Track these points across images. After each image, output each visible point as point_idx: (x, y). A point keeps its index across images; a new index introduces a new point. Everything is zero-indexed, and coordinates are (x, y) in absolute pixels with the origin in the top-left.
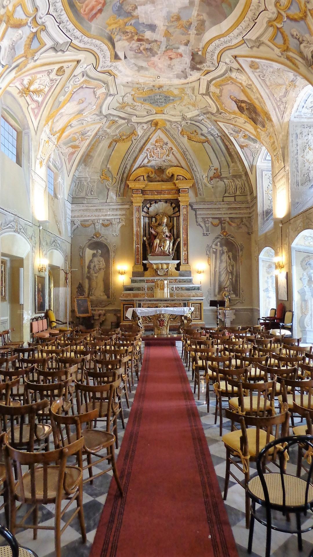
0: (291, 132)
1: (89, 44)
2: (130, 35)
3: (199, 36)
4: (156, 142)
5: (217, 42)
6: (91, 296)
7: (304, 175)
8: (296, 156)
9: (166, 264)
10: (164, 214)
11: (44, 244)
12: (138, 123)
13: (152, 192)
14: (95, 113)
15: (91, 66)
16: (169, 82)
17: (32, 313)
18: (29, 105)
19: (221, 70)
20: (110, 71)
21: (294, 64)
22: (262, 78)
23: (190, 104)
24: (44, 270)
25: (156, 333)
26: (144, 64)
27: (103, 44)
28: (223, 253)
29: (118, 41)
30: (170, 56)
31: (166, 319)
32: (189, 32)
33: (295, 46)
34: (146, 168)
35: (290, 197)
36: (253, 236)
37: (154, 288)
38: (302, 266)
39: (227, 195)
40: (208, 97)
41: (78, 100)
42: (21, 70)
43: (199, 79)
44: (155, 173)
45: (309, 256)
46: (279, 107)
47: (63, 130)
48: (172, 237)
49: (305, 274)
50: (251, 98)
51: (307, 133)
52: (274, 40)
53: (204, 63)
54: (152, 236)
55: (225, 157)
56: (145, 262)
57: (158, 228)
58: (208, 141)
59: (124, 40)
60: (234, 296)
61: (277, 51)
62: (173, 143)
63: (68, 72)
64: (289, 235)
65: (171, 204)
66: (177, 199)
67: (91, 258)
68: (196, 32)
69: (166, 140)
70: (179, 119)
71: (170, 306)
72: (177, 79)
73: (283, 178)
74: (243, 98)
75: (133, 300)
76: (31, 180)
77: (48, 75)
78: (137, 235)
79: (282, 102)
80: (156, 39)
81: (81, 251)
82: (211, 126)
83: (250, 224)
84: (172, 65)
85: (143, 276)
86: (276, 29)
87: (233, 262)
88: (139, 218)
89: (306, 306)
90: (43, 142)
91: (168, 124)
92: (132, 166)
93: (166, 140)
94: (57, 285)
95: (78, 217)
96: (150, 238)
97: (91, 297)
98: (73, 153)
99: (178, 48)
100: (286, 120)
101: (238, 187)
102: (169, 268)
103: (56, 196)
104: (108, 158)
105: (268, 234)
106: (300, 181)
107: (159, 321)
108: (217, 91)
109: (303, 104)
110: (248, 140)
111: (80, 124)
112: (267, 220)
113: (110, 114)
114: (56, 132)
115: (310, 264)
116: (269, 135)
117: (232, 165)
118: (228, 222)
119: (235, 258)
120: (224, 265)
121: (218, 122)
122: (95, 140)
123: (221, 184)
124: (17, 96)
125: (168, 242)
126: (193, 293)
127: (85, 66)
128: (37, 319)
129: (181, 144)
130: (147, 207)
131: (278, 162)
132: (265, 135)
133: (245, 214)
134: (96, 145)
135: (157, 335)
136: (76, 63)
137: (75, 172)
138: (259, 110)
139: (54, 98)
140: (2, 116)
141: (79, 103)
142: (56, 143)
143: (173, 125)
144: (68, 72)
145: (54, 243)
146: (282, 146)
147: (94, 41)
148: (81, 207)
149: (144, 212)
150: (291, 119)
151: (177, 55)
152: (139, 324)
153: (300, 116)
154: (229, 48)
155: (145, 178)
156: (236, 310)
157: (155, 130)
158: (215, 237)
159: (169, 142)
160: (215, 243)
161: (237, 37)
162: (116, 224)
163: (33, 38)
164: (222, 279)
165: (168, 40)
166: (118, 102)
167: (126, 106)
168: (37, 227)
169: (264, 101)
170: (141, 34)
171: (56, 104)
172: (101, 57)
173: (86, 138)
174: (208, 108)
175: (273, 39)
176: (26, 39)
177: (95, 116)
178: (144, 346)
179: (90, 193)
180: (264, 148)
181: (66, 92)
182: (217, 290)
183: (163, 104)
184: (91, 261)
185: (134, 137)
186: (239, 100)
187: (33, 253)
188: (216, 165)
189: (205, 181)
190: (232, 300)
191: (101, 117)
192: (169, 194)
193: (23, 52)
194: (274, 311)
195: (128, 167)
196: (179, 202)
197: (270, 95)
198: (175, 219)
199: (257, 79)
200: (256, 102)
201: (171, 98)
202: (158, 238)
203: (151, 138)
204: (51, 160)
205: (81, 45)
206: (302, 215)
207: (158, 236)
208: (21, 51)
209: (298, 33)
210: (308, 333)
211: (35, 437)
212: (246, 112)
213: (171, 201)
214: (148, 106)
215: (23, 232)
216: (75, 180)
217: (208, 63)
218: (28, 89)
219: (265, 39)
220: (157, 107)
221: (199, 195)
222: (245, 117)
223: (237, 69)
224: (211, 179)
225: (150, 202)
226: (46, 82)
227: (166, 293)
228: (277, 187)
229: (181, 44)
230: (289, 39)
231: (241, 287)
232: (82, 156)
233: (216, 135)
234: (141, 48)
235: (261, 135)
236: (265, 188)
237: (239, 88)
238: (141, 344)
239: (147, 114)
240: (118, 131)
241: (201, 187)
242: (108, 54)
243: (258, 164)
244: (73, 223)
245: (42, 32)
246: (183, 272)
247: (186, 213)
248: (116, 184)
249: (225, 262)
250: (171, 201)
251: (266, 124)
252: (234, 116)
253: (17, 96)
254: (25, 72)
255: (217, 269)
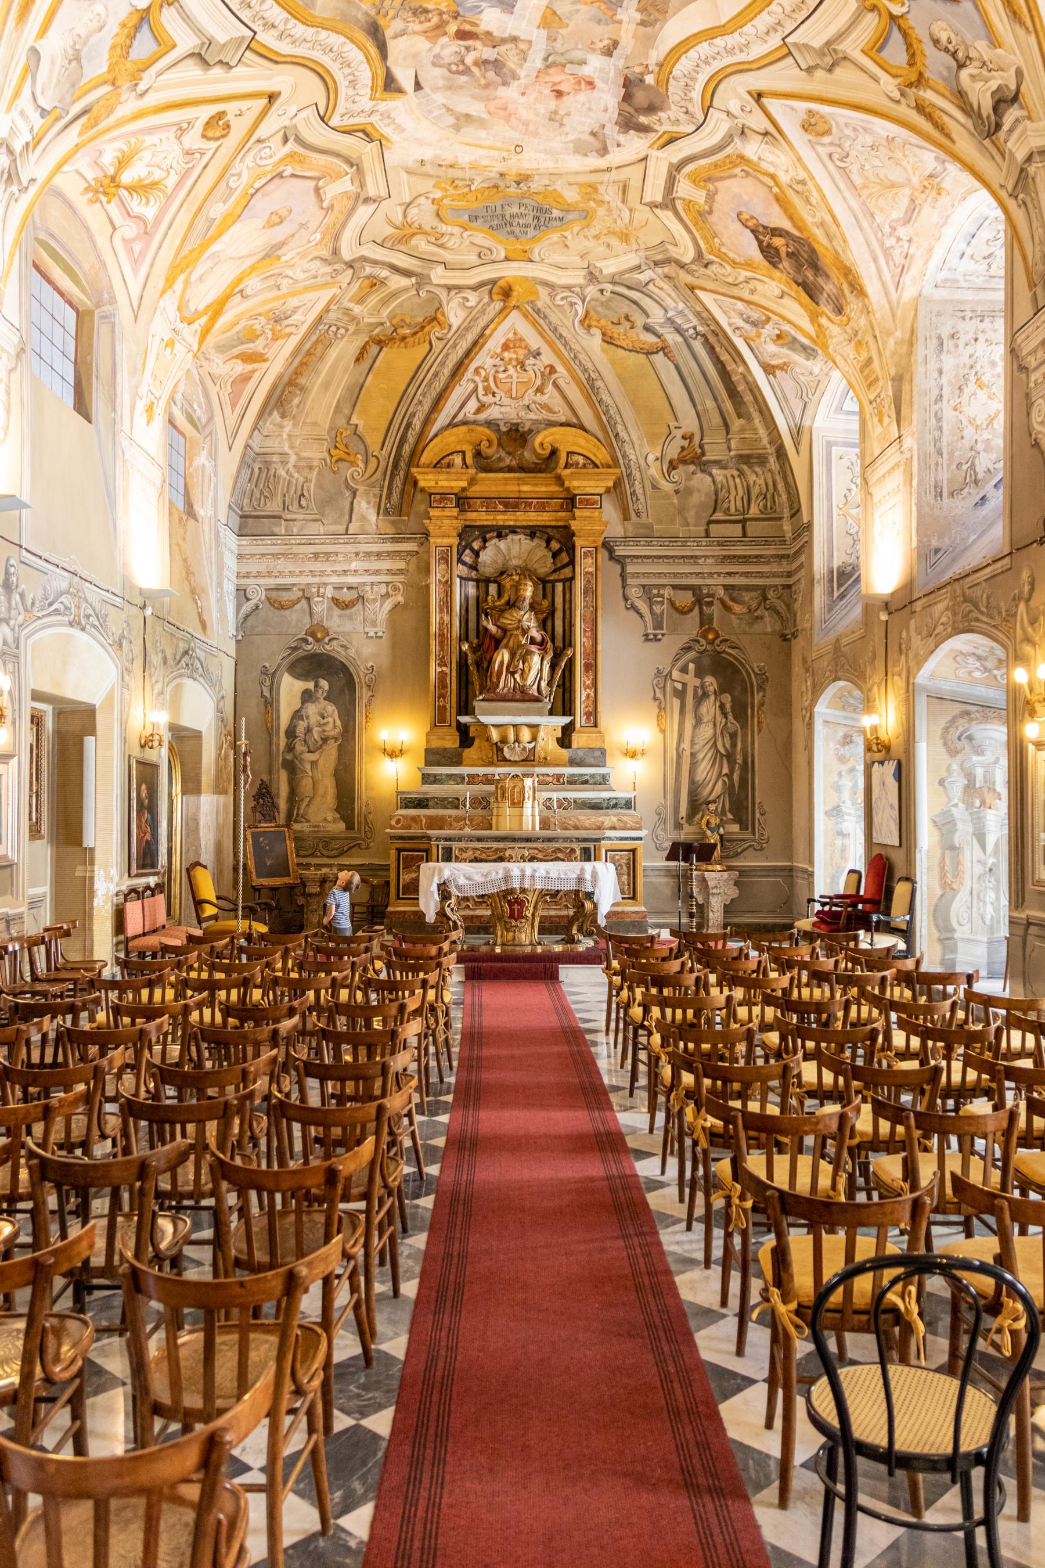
0: (921, 335)
1: (308, 45)
2: (435, 20)
3: (649, 29)
4: (506, 347)
5: (704, 49)
6: (296, 821)
7: (959, 465)
8: (937, 407)
9: (530, 726)
10: (526, 572)
11: (156, 659)
12: (449, 288)
13: (488, 502)
14: (316, 254)
15: (311, 112)
16: (548, 164)
17: (121, 878)
18: (114, 228)
19: (711, 134)
20: (369, 129)
21: (940, 128)
22: (839, 163)
23: (614, 233)
24: (156, 744)
25: (499, 941)
26: (476, 109)
27: (350, 46)
28: (705, 695)
29: (395, 37)
30: (555, 84)
31: (532, 898)
32: (618, 17)
33: (945, 73)
34: (471, 427)
35: (914, 531)
36: (798, 645)
37: (492, 800)
38: (945, 744)
39: (719, 516)
40: (670, 214)
41: (266, 215)
42: (96, 124)
43: (645, 159)
44: (500, 444)
45: (968, 713)
46: (887, 253)
47: (217, 309)
48: (550, 644)
49: (955, 767)
50: (803, 221)
51: (971, 335)
52: (880, 50)
53: (661, 109)
54: (487, 641)
55: (716, 399)
56: (464, 719)
57: (507, 615)
58: (664, 349)
59: (415, 33)
60: (735, 828)
61: (889, 85)
62: (557, 353)
63: (239, 128)
64: (908, 648)
65: (548, 542)
66: (567, 527)
67: (297, 705)
68: (638, 17)
69: (534, 341)
70: (577, 278)
71: (540, 856)
72: (577, 156)
73: (896, 472)
74: (777, 219)
75: (429, 838)
76: (119, 463)
77: (178, 138)
78: (442, 635)
79: (899, 239)
80: (515, 33)
81: (268, 683)
82: (675, 304)
83: (788, 606)
84: (562, 112)
85: (458, 762)
86: (885, 17)
87: (734, 725)
88: (448, 585)
89: (957, 864)
90: (155, 346)
91: (543, 292)
92: (427, 422)
93: (534, 341)
94: (192, 786)
95: (259, 575)
96: (480, 646)
97: (296, 827)
98: (245, 378)
99: (583, 62)
100: (909, 293)
101: (754, 492)
102: (540, 739)
103: (190, 511)
104: (355, 395)
105: (844, 641)
106: (945, 482)
107: (509, 902)
108: (699, 196)
109: (963, 246)
110: (790, 349)
111: (269, 288)
112: (842, 596)
113: (364, 259)
114: (198, 315)
115: (970, 738)
116: (855, 339)
117: (736, 424)
118: (721, 600)
119: (740, 711)
120: (706, 732)
121: (698, 292)
122: (314, 338)
123: (702, 482)
124: (81, 201)
125: (536, 659)
126: (609, 818)
127: (294, 109)
128: (135, 893)
129: (582, 356)
130: (472, 549)
131: (880, 421)
132: (841, 338)
133: (774, 575)
134: (318, 353)
135: (503, 944)
136: (266, 101)
137: (251, 436)
138: (826, 260)
139: (194, 210)
140: (36, 266)
141: (270, 225)
142: (195, 347)
143: (558, 297)
144: (239, 128)
145: (186, 659)
146: (893, 371)
147: (324, 34)
148: (266, 546)
149: (464, 564)
150: (924, 292)
151: (579, 83)
152: (448, 910)
153: (951, 283)
154: (741, 69)
155: (469, 460)
156: (743, 872)
157: (501, 311)
158: (680, 645)
159: (545, 350)
160: (680, 664)
161: (767, 38)
162: (375, 600)
163: (137, 28)
164: (701, 774)
165: (552, 39)
166: (390, 222)
167: (413, 235)
168: (135, 610)
169: (842, 234)
170: (469, 16)
171: (200, 225)
172: (343, 83)
173: (288, 330)
174: (670, 247)
175: (877, 47)
176: (116, 29)
177: (318, 263)
178: (462, 978)
179: (296, 504)
180: (836, 375)
181: (231, 191)
182: (683, 811)
183: (531, 232)
184: (297, 715)
185: (436, 332)
186: (765, 228)
187: (125, 691)
188: (689, 423)
189: (654, 471)
190: (729, 841)
191: (336, 266)
192: (542, 508)
193: (105, 69)
194: (855, 876)
195: (417, 423)
196: (573, 535)
197: (860, 216)
198: (559, 587)
199: (825, 166)
200: (819, 233)
201: (556, 213)
202: (506, 647)
203: (491, 335)
204: (178, 397)
205: (284, 48)
206: (949, 587)
207: (505, 641)
208: (98, 66)
209: (953, 36)
210: (961, 946)
211: (150, 1249)
212: (786, 264)
213: (549, 530)
214: (481, 239)
215: (94, 626)
216: (250, 462)
217: (674, 112)
218: (113, 179)
219: (852, 46)
220: (512, 238)
221: (633, 514)
222: (784, 277)
223: (762, 131)
224: (672, 466)
225: (485, 533)
226: (171, 157)
227: (530, 817)
228: (876, 499)
229: (594, 50)
230: (927, 52)
231: (757, 800)
232: (274, 387)
233: (691, 331)
234: (469, 60)
235: (831, 337)
236: (837, 500)
237: (766, 189)
238: (456, 976)
239: (480, 262)
240: (385, 313)
241: (639, 491)
242: (365, 75)
243: (817, 424)
244: (242, 594)
245: (164, 10)
246: (580, 753)
247: (592, 569)
248: (378, 475)
249: (711, 725)
250: (549, 530)
251: (848, 303)
252: (750, 274)
253: (81, 201)
254: (108, 130)
255: (686, 745)
